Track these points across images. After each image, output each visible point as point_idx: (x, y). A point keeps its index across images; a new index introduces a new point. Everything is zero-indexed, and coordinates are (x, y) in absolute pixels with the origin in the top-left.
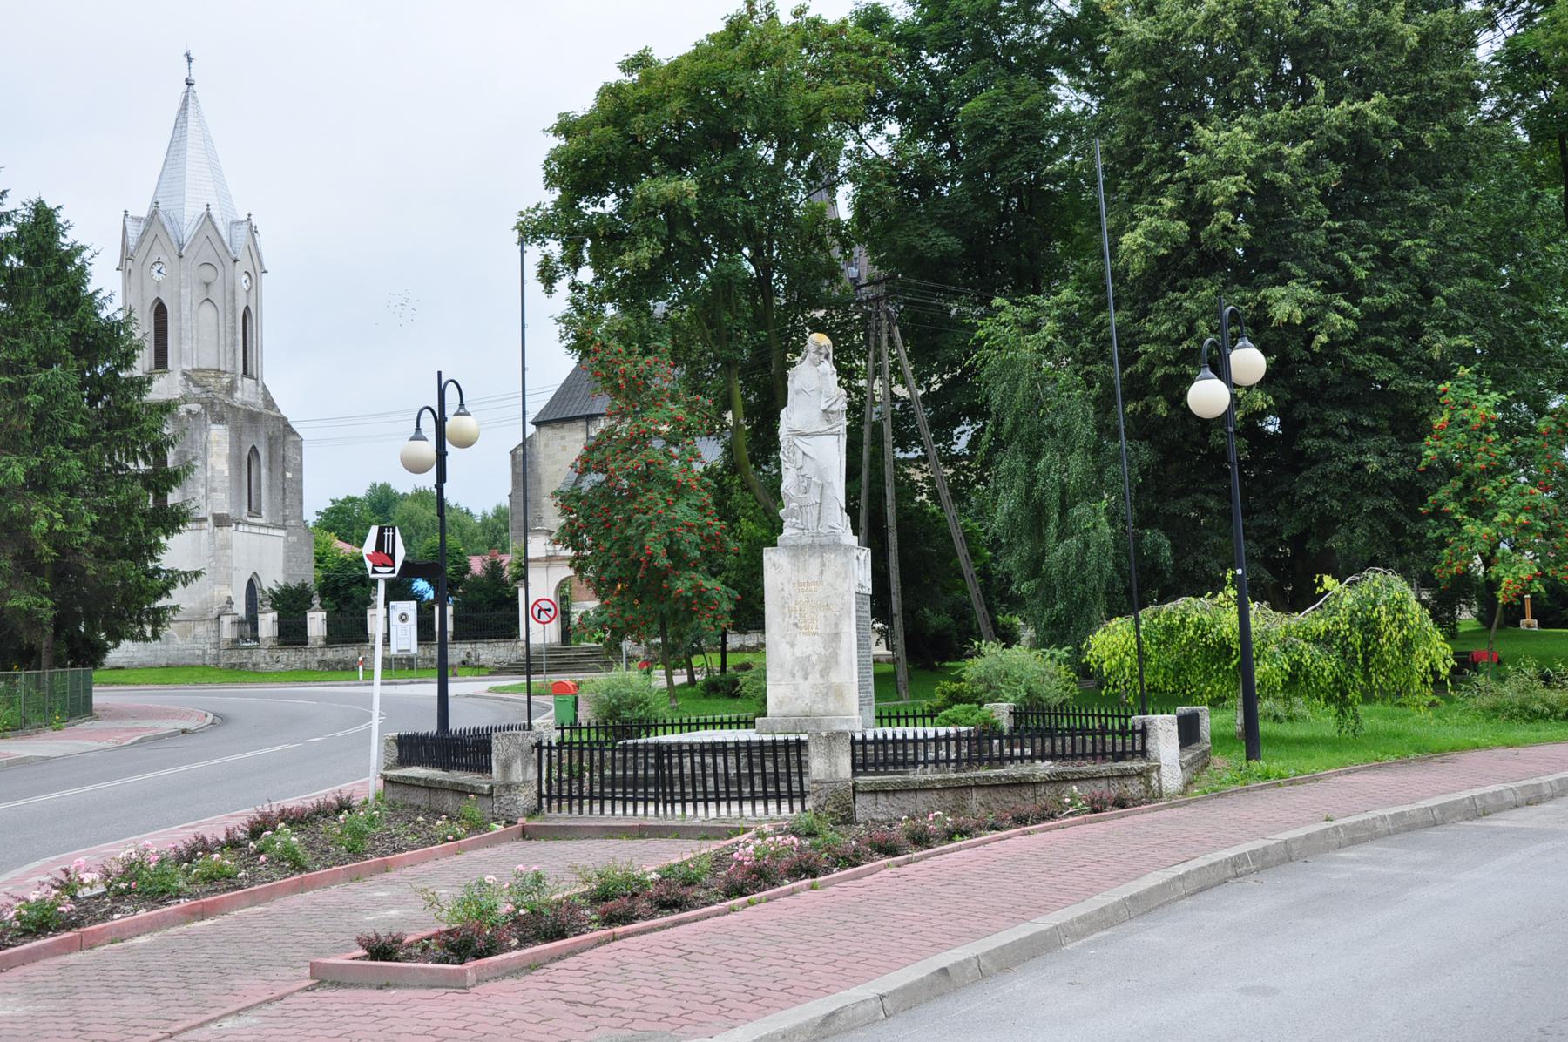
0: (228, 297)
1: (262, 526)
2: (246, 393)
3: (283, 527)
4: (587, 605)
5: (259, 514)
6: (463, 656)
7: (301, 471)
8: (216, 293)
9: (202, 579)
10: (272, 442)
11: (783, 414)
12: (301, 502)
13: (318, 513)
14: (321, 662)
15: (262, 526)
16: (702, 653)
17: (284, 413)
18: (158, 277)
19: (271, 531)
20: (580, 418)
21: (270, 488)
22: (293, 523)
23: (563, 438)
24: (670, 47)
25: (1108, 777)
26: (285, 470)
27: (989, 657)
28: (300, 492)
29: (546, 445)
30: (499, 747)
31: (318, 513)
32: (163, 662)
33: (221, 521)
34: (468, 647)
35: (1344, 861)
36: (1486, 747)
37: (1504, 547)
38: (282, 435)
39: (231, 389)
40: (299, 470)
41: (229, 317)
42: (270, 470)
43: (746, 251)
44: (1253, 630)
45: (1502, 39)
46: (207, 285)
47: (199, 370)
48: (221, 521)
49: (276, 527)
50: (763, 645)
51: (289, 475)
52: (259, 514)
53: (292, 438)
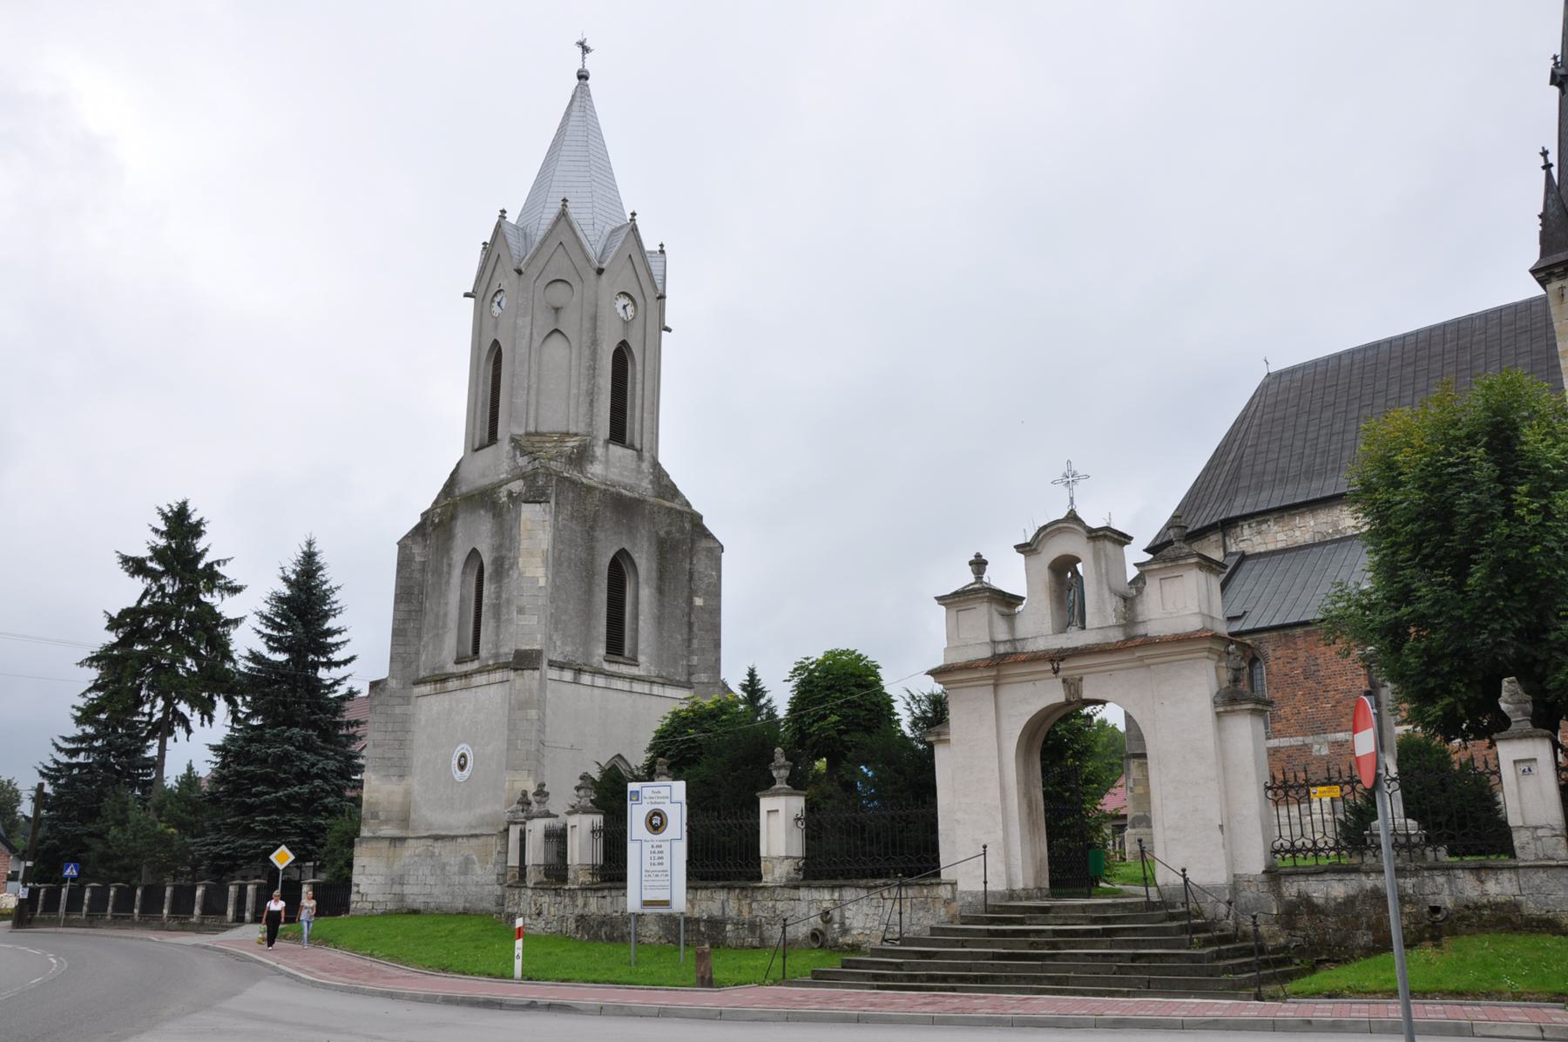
0: (587, 324)
1: (633, 679)
2: (610, 467)
3: (688, 685)
4: (228, 665)
5: (634, 661)
7: (718, 595)
8: (569, 323)
10: (666, 551)
12: (717, 645)
14: (581, 919)
15: (633, 679)
17: (696, 507)
18: (496, 310)
19: (657, 690)
21: (660, 621)
22: (704, 677)
26: (692, 593)
28: (715, 629)
32: (460, 905)
33: (524, 661)
34: (825, 897)
38: (685, 543)
39: (581, 456)
40: (715, 592)
41: (586, 352)
42: (660, 591)
46: (557, 310)
47: (537, 434)
48: (524, 661)
49: (668, 682)
51: (698, 602)
52: (634, 661)
53: (704, 544)
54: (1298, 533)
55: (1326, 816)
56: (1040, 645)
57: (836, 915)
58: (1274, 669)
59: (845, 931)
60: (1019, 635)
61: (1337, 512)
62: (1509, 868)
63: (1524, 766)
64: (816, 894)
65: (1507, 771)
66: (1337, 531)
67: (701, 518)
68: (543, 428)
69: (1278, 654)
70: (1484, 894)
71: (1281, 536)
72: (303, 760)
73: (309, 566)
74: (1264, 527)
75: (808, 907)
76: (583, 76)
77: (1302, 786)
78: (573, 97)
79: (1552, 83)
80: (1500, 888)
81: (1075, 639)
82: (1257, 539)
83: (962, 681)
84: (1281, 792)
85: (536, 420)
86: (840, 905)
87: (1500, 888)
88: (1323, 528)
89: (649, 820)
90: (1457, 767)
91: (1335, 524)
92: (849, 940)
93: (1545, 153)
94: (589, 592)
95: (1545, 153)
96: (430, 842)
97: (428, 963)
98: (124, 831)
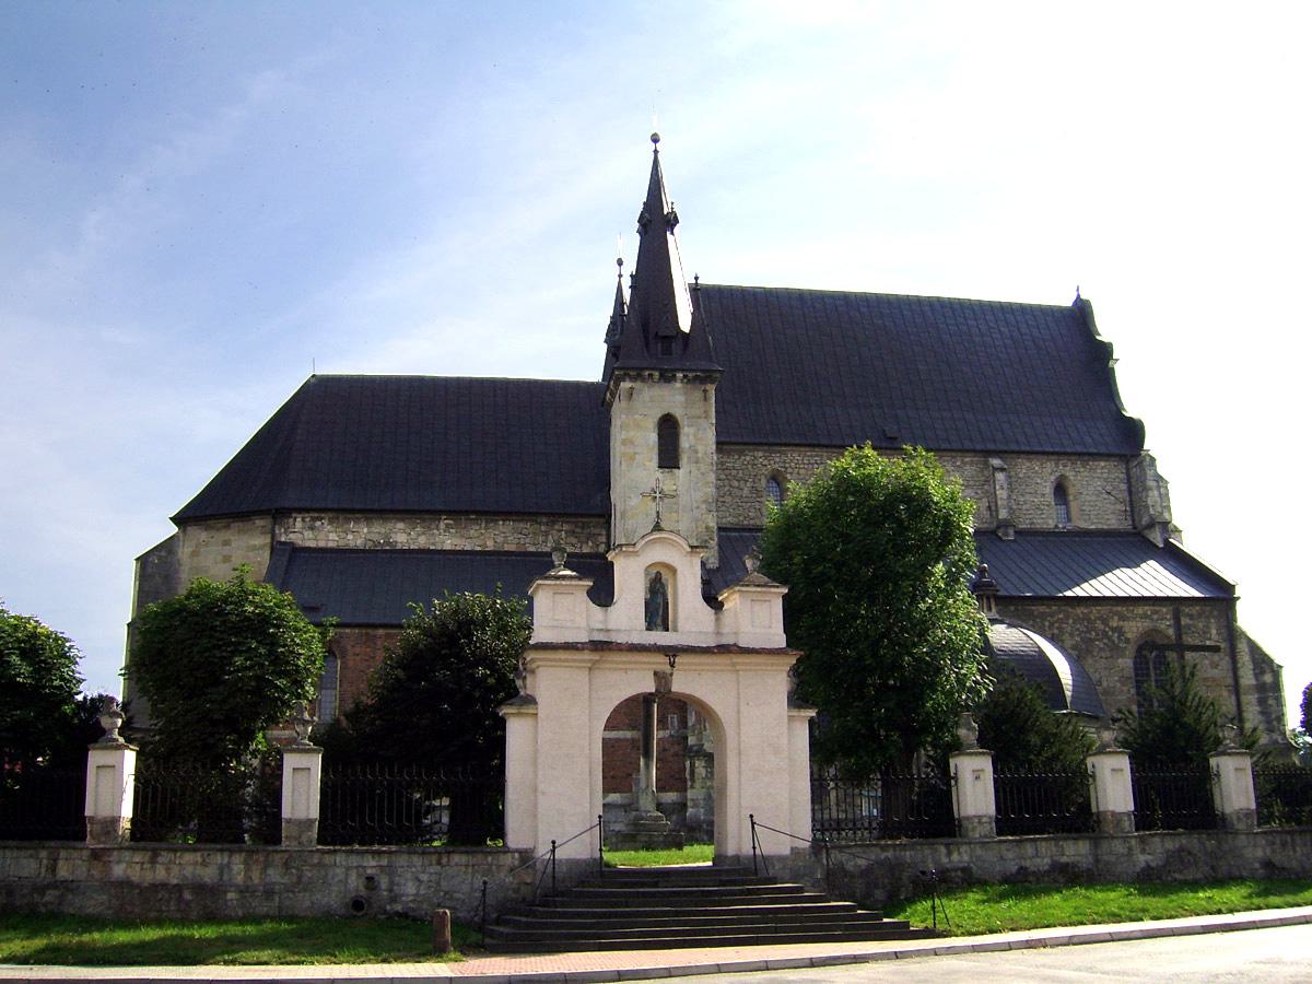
6: (355, 883)
9: (1096, 765)
11: (517, 732)
13: (1238, 598)
16: (57, 859)
20: (261, 513)
23: (226, 543)
24: (1301, 702)
25: (121, 848)
27: (312, 689)
29: (195, 554)
30: (225, 553)
31: (1238, 598)
34: (1247, 650)
35: (612, 662)
36: (266, 963)
37: (414, 869)
43: (499, 584)
44: (1115, 527)
45: (380, 655)
50: (667, 630)
54: (350, 537)
55: (1063, 332)
56: (636, 639)
57: (384, 882)
58: (351, 663)
59: (394, 899)
60: (611, 626)
61: (390, 525)
62: (966, 843)
63: (976, 774)
64: (354, 860)
65: (1107, 772)
66: (389, 543)
67: (1301, 706)
68: (610, 627)
69: (357, 650)
70: (950, 861)
71: (332, 536)
72: (1105, 644)
73: (171, 519)
74: (318, 523)
75: (347, 871)
76: (656, 152)
77: (827, 830)
78: (288, 964)
79: (137, 559)
80: (654, 667)
81: (659, 637)
82: (308, 534)
83: (555, 660)
84: (826, 825)
85: (293, 807)
86: (389, 870)
87: (654, 667)
88: (375, 537)
89: (225, 541)
90: (674, 817)
91: (387, 536)
92: (399, 908)
93: (620, 262)
94: (770, 592)
95: (620, 262)
96: (1230, 681)
97: (1151, 687)
98: (603, 594)
